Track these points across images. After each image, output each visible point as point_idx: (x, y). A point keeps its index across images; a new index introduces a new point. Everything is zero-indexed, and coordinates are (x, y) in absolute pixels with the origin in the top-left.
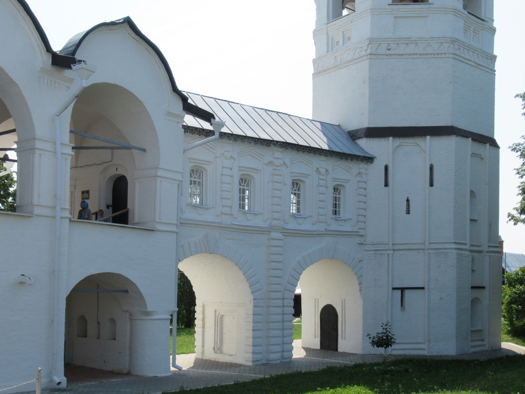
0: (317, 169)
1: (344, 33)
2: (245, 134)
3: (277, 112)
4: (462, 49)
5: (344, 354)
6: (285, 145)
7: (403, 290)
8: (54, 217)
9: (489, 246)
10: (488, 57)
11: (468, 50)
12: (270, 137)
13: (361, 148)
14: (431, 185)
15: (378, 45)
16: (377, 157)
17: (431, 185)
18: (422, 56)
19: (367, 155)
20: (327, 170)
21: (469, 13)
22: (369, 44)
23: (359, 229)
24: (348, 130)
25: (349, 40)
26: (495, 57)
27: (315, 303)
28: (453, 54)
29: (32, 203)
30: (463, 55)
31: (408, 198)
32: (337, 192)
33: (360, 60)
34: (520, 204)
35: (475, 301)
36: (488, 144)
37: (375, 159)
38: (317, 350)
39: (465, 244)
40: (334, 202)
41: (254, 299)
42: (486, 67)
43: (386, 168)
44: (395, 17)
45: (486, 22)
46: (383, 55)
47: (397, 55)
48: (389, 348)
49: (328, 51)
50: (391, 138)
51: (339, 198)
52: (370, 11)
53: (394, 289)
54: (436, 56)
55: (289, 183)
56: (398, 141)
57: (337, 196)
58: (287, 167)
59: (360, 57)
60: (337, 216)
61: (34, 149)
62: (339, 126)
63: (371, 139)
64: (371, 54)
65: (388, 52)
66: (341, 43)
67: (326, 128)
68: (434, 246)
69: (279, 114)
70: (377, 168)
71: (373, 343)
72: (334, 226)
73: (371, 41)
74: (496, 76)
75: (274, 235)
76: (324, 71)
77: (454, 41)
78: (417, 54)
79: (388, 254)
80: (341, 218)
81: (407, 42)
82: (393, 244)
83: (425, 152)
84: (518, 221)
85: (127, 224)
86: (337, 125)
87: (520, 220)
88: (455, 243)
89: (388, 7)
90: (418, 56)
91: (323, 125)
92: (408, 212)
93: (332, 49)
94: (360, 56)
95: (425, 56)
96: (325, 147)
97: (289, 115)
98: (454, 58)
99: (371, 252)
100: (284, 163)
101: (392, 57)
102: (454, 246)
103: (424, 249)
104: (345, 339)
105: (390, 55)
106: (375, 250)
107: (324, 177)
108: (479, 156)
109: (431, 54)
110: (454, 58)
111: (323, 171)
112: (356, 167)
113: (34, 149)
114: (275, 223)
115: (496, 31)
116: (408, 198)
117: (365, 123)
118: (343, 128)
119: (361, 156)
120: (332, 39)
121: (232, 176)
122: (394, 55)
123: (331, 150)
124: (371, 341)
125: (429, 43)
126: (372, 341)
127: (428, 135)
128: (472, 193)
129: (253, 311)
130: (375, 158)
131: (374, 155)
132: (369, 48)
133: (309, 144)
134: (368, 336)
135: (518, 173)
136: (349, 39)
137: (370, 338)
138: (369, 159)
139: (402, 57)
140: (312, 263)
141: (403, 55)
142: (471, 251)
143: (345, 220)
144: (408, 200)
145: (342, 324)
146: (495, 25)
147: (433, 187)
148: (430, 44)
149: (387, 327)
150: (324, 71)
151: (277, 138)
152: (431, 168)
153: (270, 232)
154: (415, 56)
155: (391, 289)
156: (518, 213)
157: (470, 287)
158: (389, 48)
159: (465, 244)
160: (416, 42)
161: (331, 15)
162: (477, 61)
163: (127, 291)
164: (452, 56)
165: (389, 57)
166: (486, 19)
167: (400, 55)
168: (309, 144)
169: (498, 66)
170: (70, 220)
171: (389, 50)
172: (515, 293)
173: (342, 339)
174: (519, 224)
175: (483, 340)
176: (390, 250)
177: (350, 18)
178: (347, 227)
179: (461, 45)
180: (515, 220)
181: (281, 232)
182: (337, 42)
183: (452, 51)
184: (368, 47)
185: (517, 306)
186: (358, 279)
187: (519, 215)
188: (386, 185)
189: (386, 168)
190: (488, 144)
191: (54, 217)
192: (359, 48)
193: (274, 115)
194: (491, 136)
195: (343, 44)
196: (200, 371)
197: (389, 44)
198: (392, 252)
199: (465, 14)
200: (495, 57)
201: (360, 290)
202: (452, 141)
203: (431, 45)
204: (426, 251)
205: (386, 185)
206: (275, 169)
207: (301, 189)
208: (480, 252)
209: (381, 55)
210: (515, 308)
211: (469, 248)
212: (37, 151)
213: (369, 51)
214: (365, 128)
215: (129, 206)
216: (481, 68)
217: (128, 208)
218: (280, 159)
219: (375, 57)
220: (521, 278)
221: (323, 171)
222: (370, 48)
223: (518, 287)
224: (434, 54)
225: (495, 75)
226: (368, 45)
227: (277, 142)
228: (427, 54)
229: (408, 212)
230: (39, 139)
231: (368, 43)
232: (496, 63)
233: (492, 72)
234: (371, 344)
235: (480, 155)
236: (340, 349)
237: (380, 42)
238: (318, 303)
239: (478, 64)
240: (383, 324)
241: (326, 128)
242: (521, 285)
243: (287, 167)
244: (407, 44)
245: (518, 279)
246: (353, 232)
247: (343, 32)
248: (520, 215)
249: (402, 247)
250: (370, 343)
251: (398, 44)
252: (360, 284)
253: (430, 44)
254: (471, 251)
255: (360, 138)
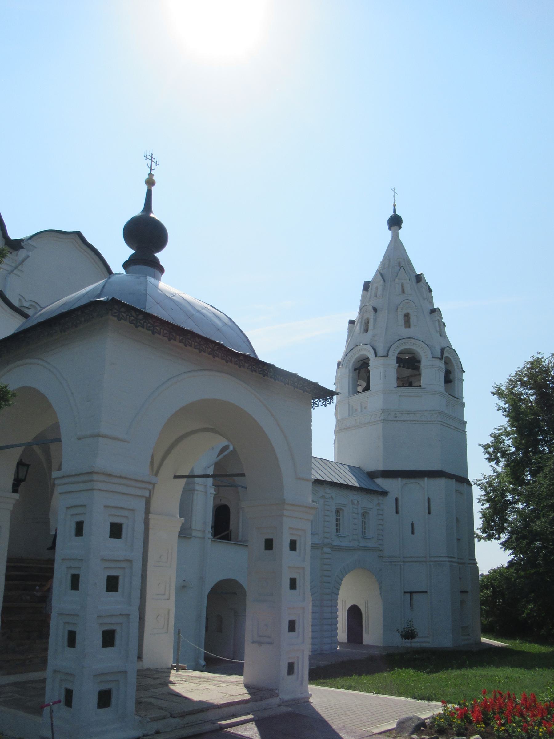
0: (352, 500)
1: (362, 404)
2: (316, 477)
3: (321, 459)
4: (445, 417)
5: (369, 647)
6: (333, 484)
7: (411, 593)
8: (204, 538)
9: (470, 559)
10: (450, 418)
11: (452, 420)
12: (344, 481)
13: (378, 485)
14: (429, 513)
15: (388, 414)
16: (390, 492)
17: (429, 513)
18: (419, 422)
19: (383, 491)
20: (358, 502)
21: (449, 394)
22: (382, 413)
23: (379, 545)
24: (367, 471)
25: (365, 409)
26: (466, 422)
27: (343, 604)
28: (440, 421)
29: (190, 527)
30: (446, 422)
31: (412, 522)
32: (338, 514)
33: (375, 423)
34: (482, 525)
35: (463, 602)
36: (465, 484)
37: (388, 493)
38: (345, 643)
39: (454, 558)
40: (338, 523)
41: (313, 600)
42: (460, 429)
43: (397, 500)
44: (399, 396)
45: (459, 399)
46: (392, 421)
47: (401, 421)
48: (414, 640)
49: (349, 415)
50: (400, 479)
51: (340, 519)
52: (382, 391)
53: (405, 592)
54: (429, 422)
55: (334, 511)
56: (405, 481)
57: (338, 517)
58: (333, 499)
59: (375, 421)
60: (338, 533)
61: (194, 490)
62: (359, 468)
63: (386, 479)
64: (383, 420)
65: (395, 419)
66: (359, 410)
67: (355, 470)
68: (433, 559)
69: (322, 460)
70: (389, 501)
71: (402, 636)
72: (363, 543)
73: (383, 411)
74: (467, 435)
75: (326, 550)
76: (347, 429)
77: (441, 413)
78: (415, 421)
79: (400, 565)
80: (366, 536)
81: (408, 413)
82: (404, 557)
83: (424, 489)
84: (481, 539)
85: (230, 540)
86: (358, 467)
87: (483, 538)
88: (448, 557)
89: (394, 389)
90: (417, 422)
91: (351, 469)
92: (413, 533)
93: (352, 414)
94: (376, 420)
95: (421, 422)
96: (357, 485)
97: (328, 461)
98: (441, 424)
99: (388, 563)
100: (332, 497)
101: (398, 422)
102: (447, 559)
103: (425, 562)
104: (368, 633)
105: (397, 421)
106: (391, 562)
107: (356, 507)
108: (459, 492)
109: (425, 421)
110: (441, 424)
111: (355, 502)
112: (376, 499)
113: (194, 490)
114: (326, 541)
115: (465, 405)
116: (412, 522)
117: (380, 467)
118: (363, 469)
119: (380, 491)
120: (352, 407)
121: (358, 514)
122: (399, 421)
123: (361, 487)
124: (400, 635)
125: (423, 414)
126: (401, 634)
127: (426, 477)
128: (457, 520)
129: (312, 609)
130: (389, 492)
131: (387, 490)
132: (382, 416)
133: (324, 478)
134: (397, 631)
135: (479, 502)
136: (365, 408)
137: (399, 632)
138: (384, 493)
139: (404, 422)
140: (349, 572)
141: (406, 421)
142: (459, 563)
143: (370, 539)
144: (412, 524)
145: (366, 621)
146: (464, 401)
147: (430, 515)
148: (424, 414)
149: (411, 623)
150: (347, 429)
151: (328, 479)
152: (429, 500)
153: (323, 547)
154: (414, 422)
155: (403, 592)
156: (481, 532)
157: (459, 592)
158: (396, 416)
159: (454, 558)
160: (415, 413)
161: (351, 392)
162: (454, 425)
163: (235, 593)
164: (440, 423)
165: (396, 422)
166: (459, 398)
167: (403, 421)
168: (324, 478)
169: (468, 428)
170: (211, 540)
171: (396, 417)
172: (483, 596)
173: (366, 633)
174: (482, 541)
175: (468, 635)
176: (402, 562)
177: (435, 421)
178: (371, 544)
179: (445, 415)
180: (478, 538)
181: (330, 548)
182: (356, 409)
183: (439, 420)
184: (381, 415)
185: (486, 607)
186: (379, 584)
187: (481, 534)
188: (397, 512)
189: (397, 500)
190: (465, 484)
191: (204, 538)
192: (374, 415)
193: (319, 460)
194: (465, 477)
195: (361, 411)
196: (342, 649)
197: (396, 413)
198: (402, 564)
199: (446, 395)
200: (466, 422)
201: (381, 594)
202: (442, 482)
203: (425, 415)
204: (428, 563)
205: (397, 512)
206: (326, 501)
207: (341, 514)
208: (463, 563)
209: (390, 420)
210: (484, 609)
211: (457, 561)
212: (196, 492)
213: (382, 418)
214: (380, 471)
215: (232, 527)
216: (459, 430)
217: (230, 528)
218: (329, 493)
219: (386, 422)
220: (486, 584)
221: (355, 502)
222: (383, 416)
223: (485, 591)
224: (427, 421)
225: (466, 434)
226: (381, 413)
227: (328, 481)
228: (422, 421)
229: (413, 533)
230: (197, 484)
231: (381, 412)
232: (466, 426)
233: (464, 432)
234: (400, 637)
235: (460, 491)
236: (365, 643)
237: (389, 412)
238: (345, 604)
239: (456, 428)
240: (407, 620)
241: (355, 470)
242: (487, 590)
243: (333, 499)
244: (408, 414)
245: (484, 584)
246: (375, 547)
247: (361, 403)
248: (483, 534)
249: (409, 559)
250: (400, 636)
251: (402, 414)
252: (380, 588)
253: (424, 414)
254: (459, 563)
255: (377, 477)
